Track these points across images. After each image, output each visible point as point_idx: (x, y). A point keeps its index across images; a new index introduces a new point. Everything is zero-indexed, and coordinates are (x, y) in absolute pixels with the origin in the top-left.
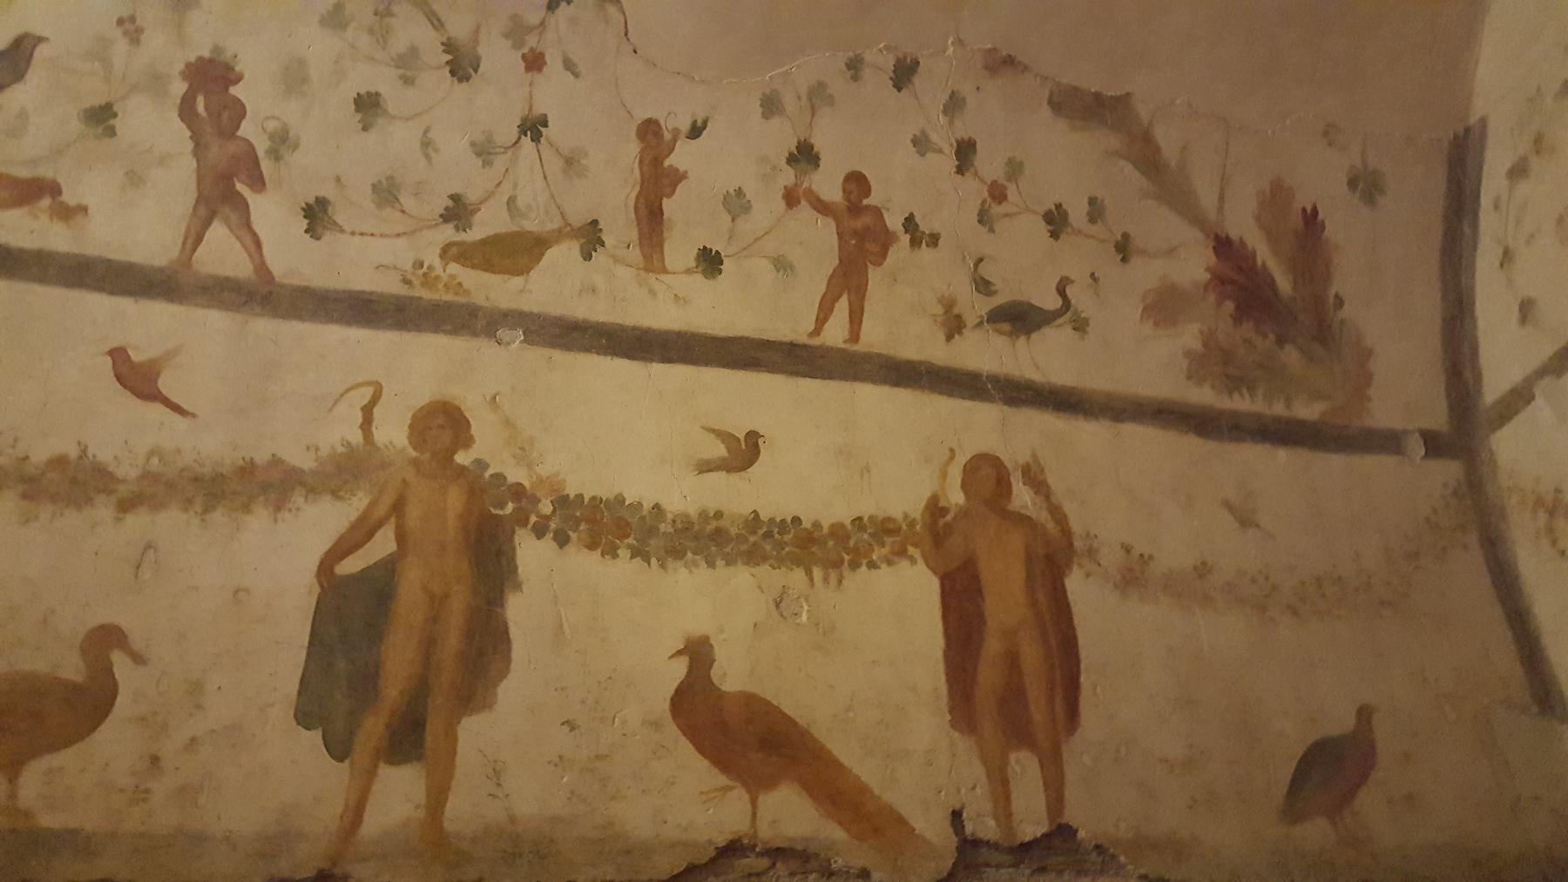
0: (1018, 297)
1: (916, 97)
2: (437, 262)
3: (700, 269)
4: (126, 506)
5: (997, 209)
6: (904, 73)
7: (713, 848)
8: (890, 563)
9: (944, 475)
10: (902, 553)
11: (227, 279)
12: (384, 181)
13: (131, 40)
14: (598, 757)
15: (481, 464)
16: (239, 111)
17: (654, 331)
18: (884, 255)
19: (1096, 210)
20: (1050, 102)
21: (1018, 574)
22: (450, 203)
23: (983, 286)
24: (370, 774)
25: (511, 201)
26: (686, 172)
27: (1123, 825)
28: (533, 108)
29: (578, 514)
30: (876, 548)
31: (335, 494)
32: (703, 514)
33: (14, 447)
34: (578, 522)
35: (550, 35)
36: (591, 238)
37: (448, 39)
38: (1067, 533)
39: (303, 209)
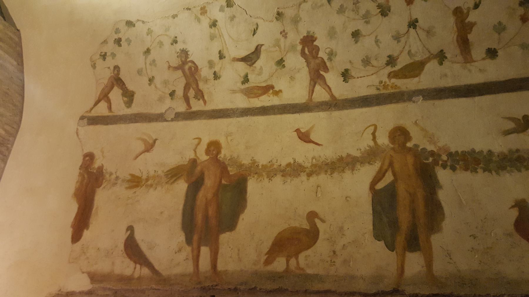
1: (99, 59)
2: (387, 80)
3: (488, 57)
4: (309, 175)
11: (323, 102)
12: (365, 58)
15: (416, 146)
16: (317, 49)
22: (388, 59)
24: (403, 256)
25: (409, 52)
28: (412, 17)
29: (458, 158)
32: (510, 151)
36: (441, 57)
39: (341, 74)
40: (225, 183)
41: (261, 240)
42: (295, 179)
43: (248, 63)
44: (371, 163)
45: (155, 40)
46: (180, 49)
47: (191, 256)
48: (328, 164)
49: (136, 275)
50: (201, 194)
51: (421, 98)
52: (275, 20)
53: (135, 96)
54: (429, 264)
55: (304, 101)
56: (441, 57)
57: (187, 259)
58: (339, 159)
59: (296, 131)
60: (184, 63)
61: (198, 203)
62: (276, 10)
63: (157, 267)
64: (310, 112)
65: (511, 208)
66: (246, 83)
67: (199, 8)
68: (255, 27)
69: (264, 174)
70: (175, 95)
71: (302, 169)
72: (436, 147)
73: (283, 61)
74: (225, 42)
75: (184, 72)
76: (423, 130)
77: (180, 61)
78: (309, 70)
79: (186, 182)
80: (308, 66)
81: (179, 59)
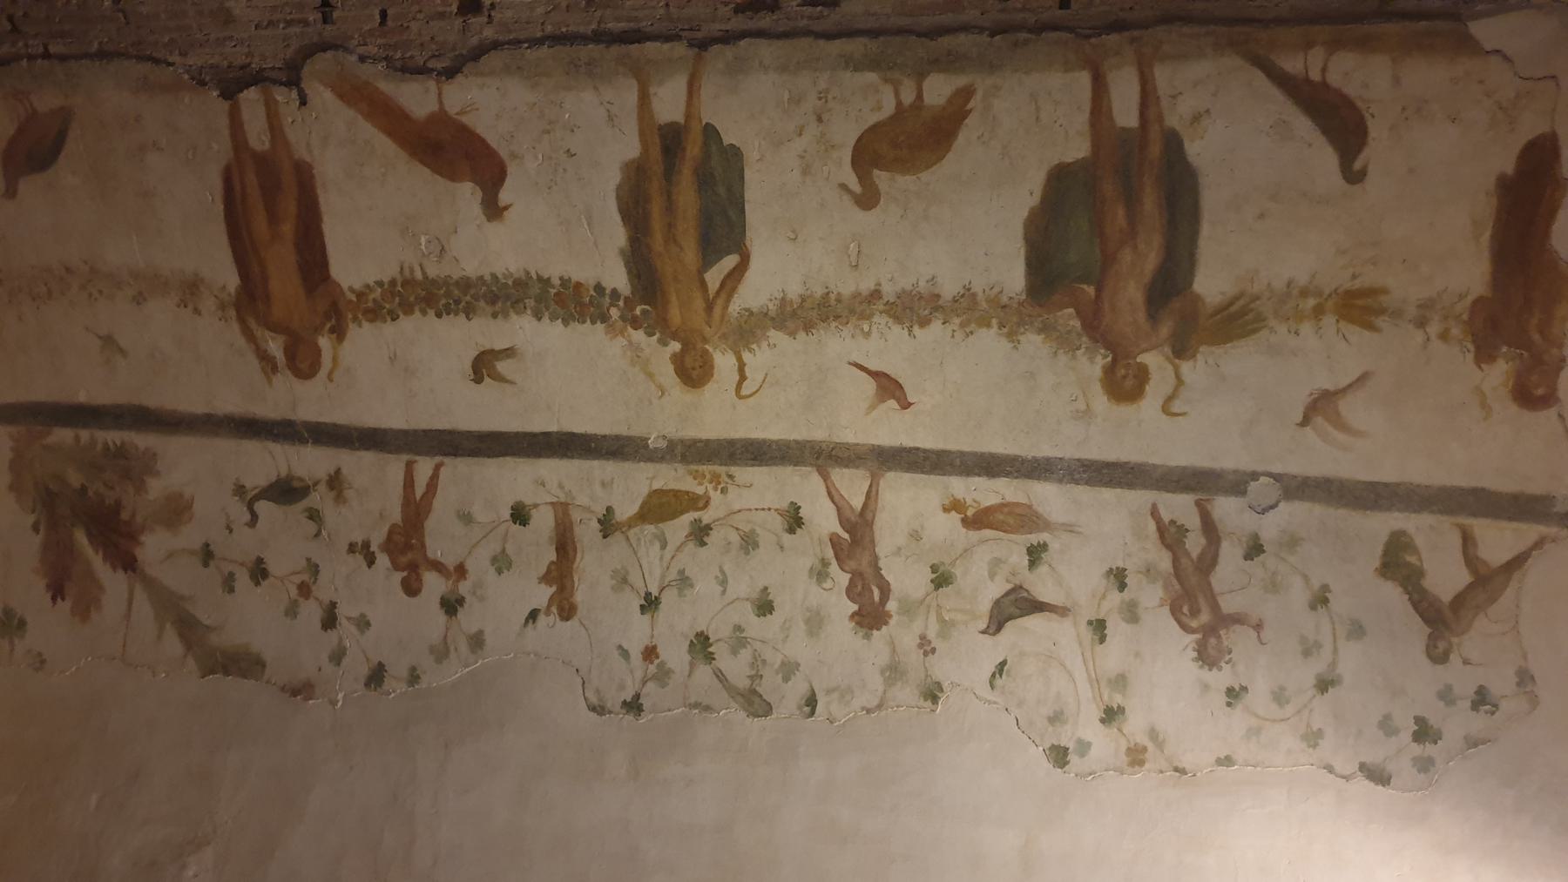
2: (712, 493)
3: (527, 508)
4: (876, 294)
5: (305, 577)
6: (376, 676)
7: (465, 73)
8: (368, 286)
9: (335, 360)
10: (360, 295)
11: (847, 466)
13: (925, 638)
14: (548, 132)
16: (850, 592)
17: (558, 457)
18: (390, 533)
19: (229, 584)
20: (264, 666)
22: (705, 539)
23: (314, 515)
24: (688, 116)
25: (663, 547)
26: (539, 583)
27: (187, 100)
29: (592, 309)
30: (379, 299)
32: (506, 316)
33: (954, 331)
34: (591, 302)
35: (639, 674)
36: (608, 525)
37: (710, 663)
38: (242, 321)
39: (803, 524)
40: (1085, 287)
41: (984, 143)
42: (909, 288)
43: (1025, 594)
44: (747, 314)
45: (1299, 712)
46: (1220, 669)
47: (1165, 103)
48: (834, 317)
50: (1151, 260)
52: (945, 685)
53: (1377, 563)
54: (644, 99)
55: (890, 475)
57: (1174, 97)
58: (812, 327)
59: (910, 404)
60: (1210, 631)
61: (1157, 241)
62: (939, 707)
63: (1260, 78)
64: (876, 447)
65: (511, 205)
66: (1036, 545)
67: (1147, 766)
68: (999, 682)
69: (984, 305)
70: (1245, 545)
71: (893, 311)
72: (629, 336)
73: (937, 582)
74: (1085, 662)
75: (1215, 607)
76: (650, 376)
77: (1224, 637)
78: (874, 546)
79: (1197, 299)
80: (876, 558)
81: (1226, 643)
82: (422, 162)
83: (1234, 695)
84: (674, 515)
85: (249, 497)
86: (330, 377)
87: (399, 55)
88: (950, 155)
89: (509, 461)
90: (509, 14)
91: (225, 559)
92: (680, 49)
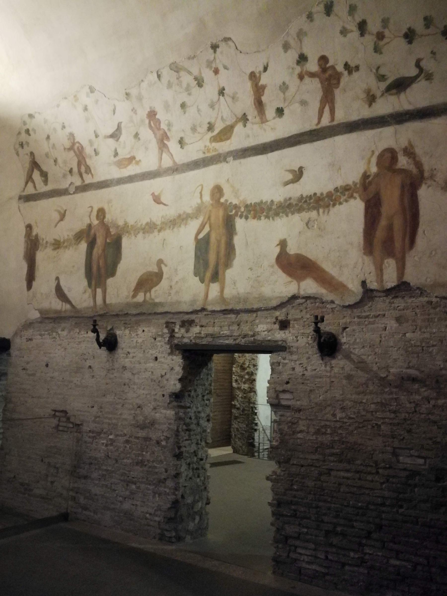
0: (398, 76)
3: (277, 116)
4: (159, 231)
5: (382, 43)
9: (369, 162)
10: (351, 196)
11: (168, 168)
14: (258, 277)
16: (159, 121)
18: (339, 83)
21: (397, 193)
23: (381, 78)
24: (208, 287)
25: (222, 117)
31: (196, 218)
32: (285, 200)
35: (218, 61)
36: (244, 119)
47: (91, 295)
49: (64, 309)
51: (232, 158)
53: (49, 175)
56: (244, 119)
60: (74, 144)
63: (74, 303)
75: (75, 152)
82: (311, 260)
83: (64, 127)
84: (221, 132)
85: (423, 75)
86: (373, 152)
87: (317, 304)
88: (138, 277)
89: (286, 135)
90: (268, 320)
91: (434, 34)
92: (210, 308)
